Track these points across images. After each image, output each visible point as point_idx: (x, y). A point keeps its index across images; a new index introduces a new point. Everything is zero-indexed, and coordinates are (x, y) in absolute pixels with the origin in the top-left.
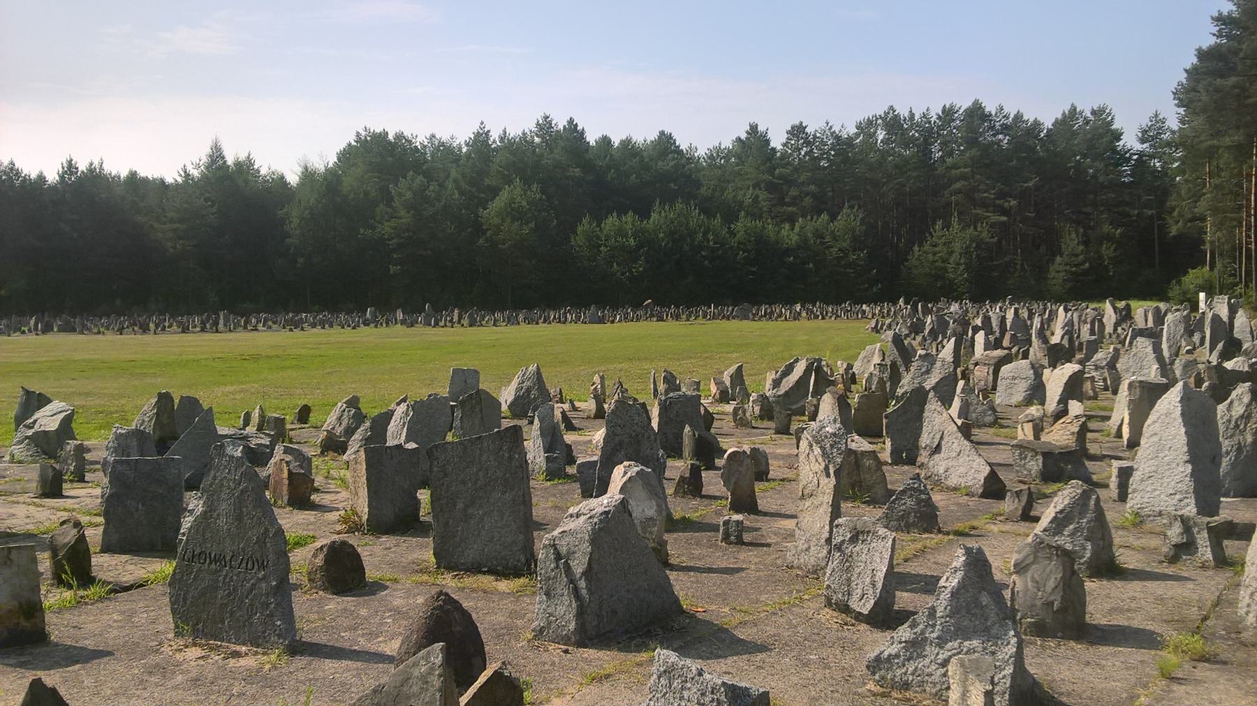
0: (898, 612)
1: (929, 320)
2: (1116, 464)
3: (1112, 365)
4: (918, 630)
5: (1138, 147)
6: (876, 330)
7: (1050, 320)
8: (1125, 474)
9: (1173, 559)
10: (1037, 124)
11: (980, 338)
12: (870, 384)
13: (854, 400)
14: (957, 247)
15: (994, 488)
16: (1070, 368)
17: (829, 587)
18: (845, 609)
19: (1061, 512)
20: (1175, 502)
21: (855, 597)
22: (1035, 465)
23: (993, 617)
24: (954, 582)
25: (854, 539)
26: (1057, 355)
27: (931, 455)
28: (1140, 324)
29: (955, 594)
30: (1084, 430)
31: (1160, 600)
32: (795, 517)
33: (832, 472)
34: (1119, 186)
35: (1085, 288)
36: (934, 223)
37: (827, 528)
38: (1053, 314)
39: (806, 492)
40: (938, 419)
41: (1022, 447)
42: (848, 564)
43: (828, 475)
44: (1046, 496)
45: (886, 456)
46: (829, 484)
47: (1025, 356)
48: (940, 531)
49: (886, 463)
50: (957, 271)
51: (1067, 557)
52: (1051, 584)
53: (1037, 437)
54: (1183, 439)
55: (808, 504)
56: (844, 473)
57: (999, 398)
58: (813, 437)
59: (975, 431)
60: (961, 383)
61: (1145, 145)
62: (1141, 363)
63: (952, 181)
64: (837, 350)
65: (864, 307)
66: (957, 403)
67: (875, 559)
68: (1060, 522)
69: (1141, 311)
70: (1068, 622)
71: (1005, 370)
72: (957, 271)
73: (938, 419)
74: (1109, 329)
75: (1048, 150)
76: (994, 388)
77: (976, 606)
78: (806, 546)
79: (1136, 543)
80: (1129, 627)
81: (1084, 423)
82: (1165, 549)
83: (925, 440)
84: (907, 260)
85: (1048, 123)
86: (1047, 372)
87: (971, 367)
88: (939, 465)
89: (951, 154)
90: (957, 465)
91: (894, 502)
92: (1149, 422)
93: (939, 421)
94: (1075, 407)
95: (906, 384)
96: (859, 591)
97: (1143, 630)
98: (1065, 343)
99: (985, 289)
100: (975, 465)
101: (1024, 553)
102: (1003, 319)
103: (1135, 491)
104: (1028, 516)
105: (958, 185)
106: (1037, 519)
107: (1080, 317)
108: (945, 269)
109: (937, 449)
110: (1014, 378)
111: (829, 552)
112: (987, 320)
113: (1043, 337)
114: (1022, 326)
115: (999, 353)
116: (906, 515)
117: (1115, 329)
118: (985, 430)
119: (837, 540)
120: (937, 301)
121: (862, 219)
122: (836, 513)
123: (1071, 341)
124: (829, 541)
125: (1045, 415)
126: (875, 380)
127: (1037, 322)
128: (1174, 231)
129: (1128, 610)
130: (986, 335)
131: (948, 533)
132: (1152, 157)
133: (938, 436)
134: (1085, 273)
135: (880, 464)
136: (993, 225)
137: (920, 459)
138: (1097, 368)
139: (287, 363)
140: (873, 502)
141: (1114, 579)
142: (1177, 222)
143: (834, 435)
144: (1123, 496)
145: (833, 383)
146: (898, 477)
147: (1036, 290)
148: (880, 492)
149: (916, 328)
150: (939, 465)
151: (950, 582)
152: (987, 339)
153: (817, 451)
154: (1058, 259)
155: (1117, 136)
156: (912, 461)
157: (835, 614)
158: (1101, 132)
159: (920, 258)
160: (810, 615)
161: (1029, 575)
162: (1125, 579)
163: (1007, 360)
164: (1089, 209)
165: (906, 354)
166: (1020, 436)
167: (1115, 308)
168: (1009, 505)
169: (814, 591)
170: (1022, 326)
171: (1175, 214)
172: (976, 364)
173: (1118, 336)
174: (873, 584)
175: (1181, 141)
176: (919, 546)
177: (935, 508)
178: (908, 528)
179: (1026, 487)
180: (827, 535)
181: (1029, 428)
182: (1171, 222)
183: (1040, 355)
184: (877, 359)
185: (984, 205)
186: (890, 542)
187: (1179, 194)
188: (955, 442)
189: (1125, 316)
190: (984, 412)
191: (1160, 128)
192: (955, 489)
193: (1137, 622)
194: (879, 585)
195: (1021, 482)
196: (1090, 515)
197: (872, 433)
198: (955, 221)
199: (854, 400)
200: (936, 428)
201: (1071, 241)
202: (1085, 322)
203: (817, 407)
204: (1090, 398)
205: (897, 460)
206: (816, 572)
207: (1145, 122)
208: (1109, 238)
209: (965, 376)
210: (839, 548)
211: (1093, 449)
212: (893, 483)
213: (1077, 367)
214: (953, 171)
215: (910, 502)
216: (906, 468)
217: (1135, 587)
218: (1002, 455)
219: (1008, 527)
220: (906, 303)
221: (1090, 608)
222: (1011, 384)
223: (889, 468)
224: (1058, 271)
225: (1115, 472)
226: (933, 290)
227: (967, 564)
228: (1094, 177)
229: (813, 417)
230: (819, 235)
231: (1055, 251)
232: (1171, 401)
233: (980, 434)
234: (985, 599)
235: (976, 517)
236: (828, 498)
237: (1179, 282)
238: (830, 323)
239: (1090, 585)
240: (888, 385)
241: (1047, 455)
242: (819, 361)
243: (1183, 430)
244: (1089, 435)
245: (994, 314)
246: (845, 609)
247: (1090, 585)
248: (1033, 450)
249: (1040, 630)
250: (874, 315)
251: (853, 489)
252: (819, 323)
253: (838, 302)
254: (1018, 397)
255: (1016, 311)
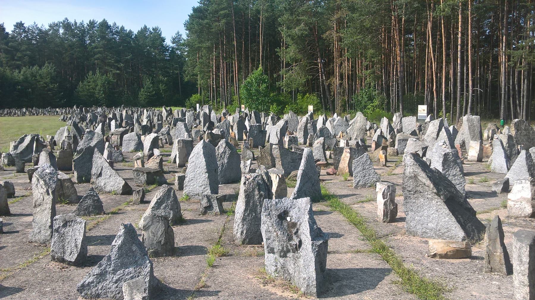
0: (89, 257)
1: (89, 116)
2: (177, 175)
3: (168, 133)
4: (103, 268)
5: (172, 45)
6: (64, 120)
7: (141, 115)
8: (182, 179)
9: (204, 213)
10: (130, 32)
11: (113, 123)
12: (64, 145)
13: (57, 153)
14: (99, 83)
15: (127, 190)
16: (153, 135)
17: (53, 251)
18: (62, 260)
19: (159, 199)
20: (202, 189)
21: (67, 254)
22: (143, 178)
23: (139, 255)
24: (119, 242)
25: (65, 225)
26: (146, 130)
27: (97, 178)
28: (176, 116)
29: (120, 248)
30: (161, 161)
31: (202, 231)
32: (32, 215)
33: (50, 192)
34: (163, 60)
35: (154, 102)
36: (88, 72)
37: (50, 220)
38: (142, 113)
39: (37, 203)
40: (100, 161)
41: (137, 170)
42: (62, 237)
43: (48, 194)
44: (149, 191)
45: (75, 179)
46: (49, 199)
47: (132, 131)
48: (104, 213)
49: (75, 183)
50: (99, 94)
51: (165, 219)
52: (160, 233)
53: (143, 166)
54: (204, 163)
55: (38, 209)
56: (56, 193)
57: (124, 149)
58: (39, 175)
59: (115, 164)
60: (107, 144)
61: (174, 45)
62: (180, 133)
63: (95, 54)
64: (45, 129)
65: (57, 109)
66: (106, 153)
67: (76, 234)
68: (159, 204)
69: (176, 111)
70: (169, 249)
71: (126, 137)
72: (99, 94)
73: (100, 161)
74: (164, 119)
75: (136, 44)
76: (121, 145)
77: (131, 252)
78: (39, 230)
79: (189, 208)
80: (192, 246)
81: (161, 158)
82: (201, 209)
83: (94, 171)
84: (76, 88)
85: (135, 32)
86: (143, 137)
87: (110, 136)
88: (101, 182)
89: (94, 42)
90: (110, 181)
91: (82, 202)
92: (190, 157)
93: (100, 161)
94: (156, 152)
95: (82, 145)
96: (69, 251)
97: (198, 246)
98: (149, 124)
99: (112, 102)
100: (118, 181)
101: (147, 221)
102: (121, 115)
103: (186, 186)
104: (144, 201)
105: (97, 56)
106: (149, 202)
107: (153, 113)
108: (94, 93)
109: (100, 175)
110: (129, 140)
111: (52, 232)
112: (114, 115)
113: (138, 121)
114: (130, 118)
115: (121, 129)
116: (88, 207)
117: (167, 119)
118: (119, 164)
119: (56, 227)
120: (91, 107)
121: (55, 69)
122: (54, 213)
123: (151, 124)
124: (51, 227)
125: (144, 156)
126: (66, 144)
127: (135, 116)
128: (186, 79)
129: (191, 238)
130: (116, 121)
131: (108, 214)
132: (177, 49)
133: (100, 169)
134: (153, 96)
135: (73, 183)
136: (114, 74)
137: (92, 180)
138: (163, 134)
139: (451, 72)
140: (71, 203)
141: (182, 225)
142: (187, 76)
143: (50, 173)
144: (181, 188)
145: (45, 146)
146: (82, 189)
147: (133, 102)
148: (73, 197)
149: (83, 119)
150: (101, 182)
151: (117, 242)
152: (116, 124)
153: (42, 182)
154: (142, 90)
155: (163, 40)
156: (88, 181)
157: (57, 264)
158: (156, 37)
159: (82, 87)
160: (44, 267)
161: (150, 230)
162: (187, 224)
163: (125, 132)
164: (154, 69)
165: (80, 132)
166: (136, 166)
167: (166, 110)
168: (135, 197)
169: (45, 253)
170: (130, 118)
171: (186, 73)
172: (112, 135)
173: (168, 121)
174: (76, 246)
175: (188, 44)
176: (96, 222)
177: (101, 203)
178: (89, 214)
179: (140, 189)
180: (49, 224)
181: (139, 162)
182: (185, 76)
183: (138, 130)
184: (66, 134)
185: (110, 65)
186: (84, 225)
187: (187, 65)
188: (108, 171)
189: (170, 113)
190: (118, 156)
191: (180, 38)
192: (109, 192)
193: (195, 243)
194: (79, 246)
195: (138, 186)
196: (171, 199)
197: (67, 169)
198: (98, 71)
199: (57, 153)
200: (99, 165)
201: (147, 82)
202: (155, 116)
203: (38, 159)
204: (161, 147)
205: (80, 181)
206: (45, 243)
207: (174, 35)
208: (162, 82)
209: (108, 140)
210: (57, 231)
211: (165, 169)
212: (80, 192)
213: (156, 135)
214: (95, 50)
215: (89, 202)
216: (85, 184)
217: (191, 226)
218: (129, 175)
219: (135, 207)
220: (77, 108)
221: (176, 240)
222: (128, 143)
223: (77, 185)
224: (142, 94)
225: (177, 178)
226: (88, 102)
227: (125, 233)
228: (155, 56)
229: (36, 163)
230: (33, 75)
231: (141, 86)
232: (198, 148)
233: (117, 166)
234: (134, 248)
235: (120, 204)
236: (49, 206)
237: (189, 100)
238: (41, 117)
239: (175, 229)
240: (72, 145)
241: (149, 173)
242: (38, 135)
243: (204, 160)
244: (164, 163)
245: (117, 112)
246: (62, 260)
247: (175, 229)
248: (142, 172)
249: (156, 254)
250: (62, 113)
251: (60, 198)
252: (35, 117)
253: (44, 107)
254: (132, 148)
255: (126, 111)
